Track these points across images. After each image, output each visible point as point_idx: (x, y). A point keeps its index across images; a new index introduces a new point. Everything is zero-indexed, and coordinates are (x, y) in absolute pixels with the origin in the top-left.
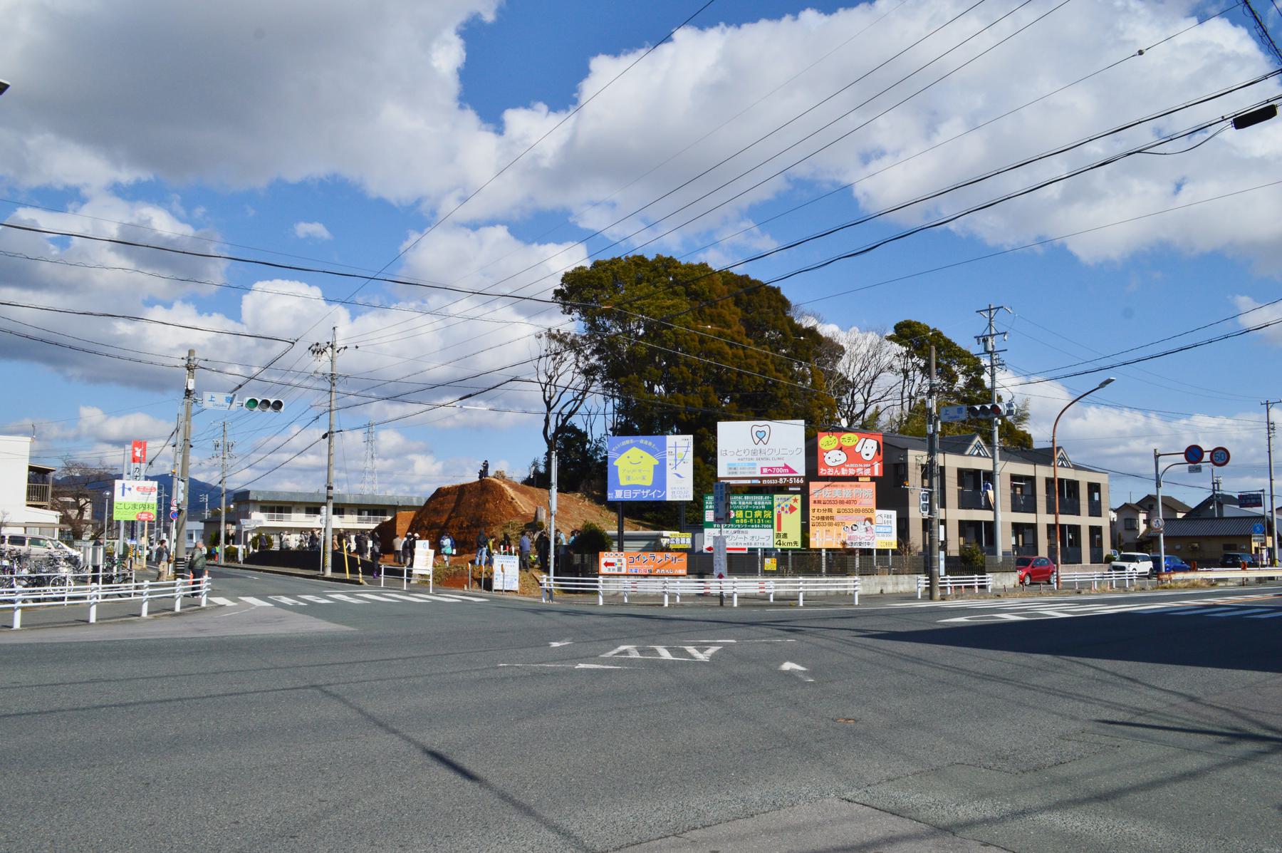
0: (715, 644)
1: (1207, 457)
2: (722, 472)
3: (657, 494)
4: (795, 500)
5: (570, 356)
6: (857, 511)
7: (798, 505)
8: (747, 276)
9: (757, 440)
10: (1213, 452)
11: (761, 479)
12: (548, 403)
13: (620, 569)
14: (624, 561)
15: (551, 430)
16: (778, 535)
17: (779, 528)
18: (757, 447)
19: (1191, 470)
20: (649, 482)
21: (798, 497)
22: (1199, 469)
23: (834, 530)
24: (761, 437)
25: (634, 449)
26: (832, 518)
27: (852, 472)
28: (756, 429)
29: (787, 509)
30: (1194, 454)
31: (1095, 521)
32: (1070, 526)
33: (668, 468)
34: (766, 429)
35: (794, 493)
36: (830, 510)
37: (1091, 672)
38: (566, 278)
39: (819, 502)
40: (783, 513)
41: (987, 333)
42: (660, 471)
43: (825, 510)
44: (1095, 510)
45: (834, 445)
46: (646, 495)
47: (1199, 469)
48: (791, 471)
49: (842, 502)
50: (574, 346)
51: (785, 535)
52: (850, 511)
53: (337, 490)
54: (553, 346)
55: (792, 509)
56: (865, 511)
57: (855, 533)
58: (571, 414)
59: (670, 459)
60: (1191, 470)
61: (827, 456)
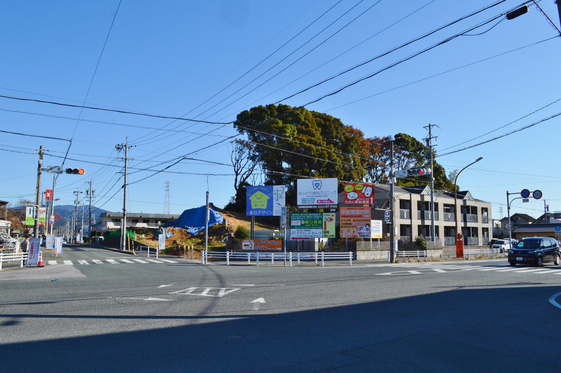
0: (238, 287)
1: (531, 195)
2: (299, 202)
3: (269, 213)
4: (333, 216)
5: (247, 151)
6: (363, 220)
7: (334, 218)
8: (325, 114)
9: (315, 187)
10: (534, 192)
11: (317, 205)
12: (236, 172)
13: (251, 248)
14: (253, 244)
15: (238, 184)
16: (325, 232)
17: (325, 229)
18: (315, 191)
19: (524, 201)
20: (265, 207)
21: (334, 214)
22: (527, 201)
23: (352, 230)
24: (317, 186)
25: (258, 192)
26: (351, 224)
27: (360, 202)
28: (315, 182)
29: (329, 220)
30: (525, 194)
31: (485, 226)
32: (472, 228)
33: (274, 201)
34: (320, 182)
35: (333, 212)
36: (350, 220)
37: (548, 282)
38: (239, 116)
39: (345, 216)
40: (327, 222)
41: (428, 137)
42: (270, 203)
43: (347, 220)
44: (486, 220)
45: (352, 190)
46: (264, 213)
47: (527, 201)
48: (331, 202)
49: (355, 216)
50: (247, 145)
51: (328, 232)
52: (359, 221)
53: (128, 211)
54: (238, 147)
55: (331, 220)
56: (366, 220)
57: (361, 231)
58: (247, 177)
59: (275, 197)
60: (524, 201)
61: (349, 195)
